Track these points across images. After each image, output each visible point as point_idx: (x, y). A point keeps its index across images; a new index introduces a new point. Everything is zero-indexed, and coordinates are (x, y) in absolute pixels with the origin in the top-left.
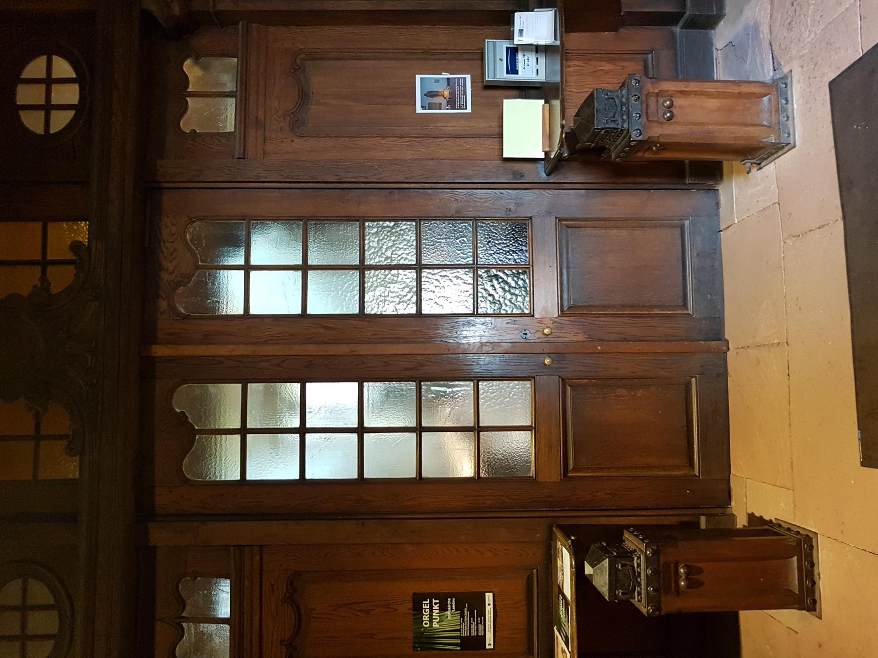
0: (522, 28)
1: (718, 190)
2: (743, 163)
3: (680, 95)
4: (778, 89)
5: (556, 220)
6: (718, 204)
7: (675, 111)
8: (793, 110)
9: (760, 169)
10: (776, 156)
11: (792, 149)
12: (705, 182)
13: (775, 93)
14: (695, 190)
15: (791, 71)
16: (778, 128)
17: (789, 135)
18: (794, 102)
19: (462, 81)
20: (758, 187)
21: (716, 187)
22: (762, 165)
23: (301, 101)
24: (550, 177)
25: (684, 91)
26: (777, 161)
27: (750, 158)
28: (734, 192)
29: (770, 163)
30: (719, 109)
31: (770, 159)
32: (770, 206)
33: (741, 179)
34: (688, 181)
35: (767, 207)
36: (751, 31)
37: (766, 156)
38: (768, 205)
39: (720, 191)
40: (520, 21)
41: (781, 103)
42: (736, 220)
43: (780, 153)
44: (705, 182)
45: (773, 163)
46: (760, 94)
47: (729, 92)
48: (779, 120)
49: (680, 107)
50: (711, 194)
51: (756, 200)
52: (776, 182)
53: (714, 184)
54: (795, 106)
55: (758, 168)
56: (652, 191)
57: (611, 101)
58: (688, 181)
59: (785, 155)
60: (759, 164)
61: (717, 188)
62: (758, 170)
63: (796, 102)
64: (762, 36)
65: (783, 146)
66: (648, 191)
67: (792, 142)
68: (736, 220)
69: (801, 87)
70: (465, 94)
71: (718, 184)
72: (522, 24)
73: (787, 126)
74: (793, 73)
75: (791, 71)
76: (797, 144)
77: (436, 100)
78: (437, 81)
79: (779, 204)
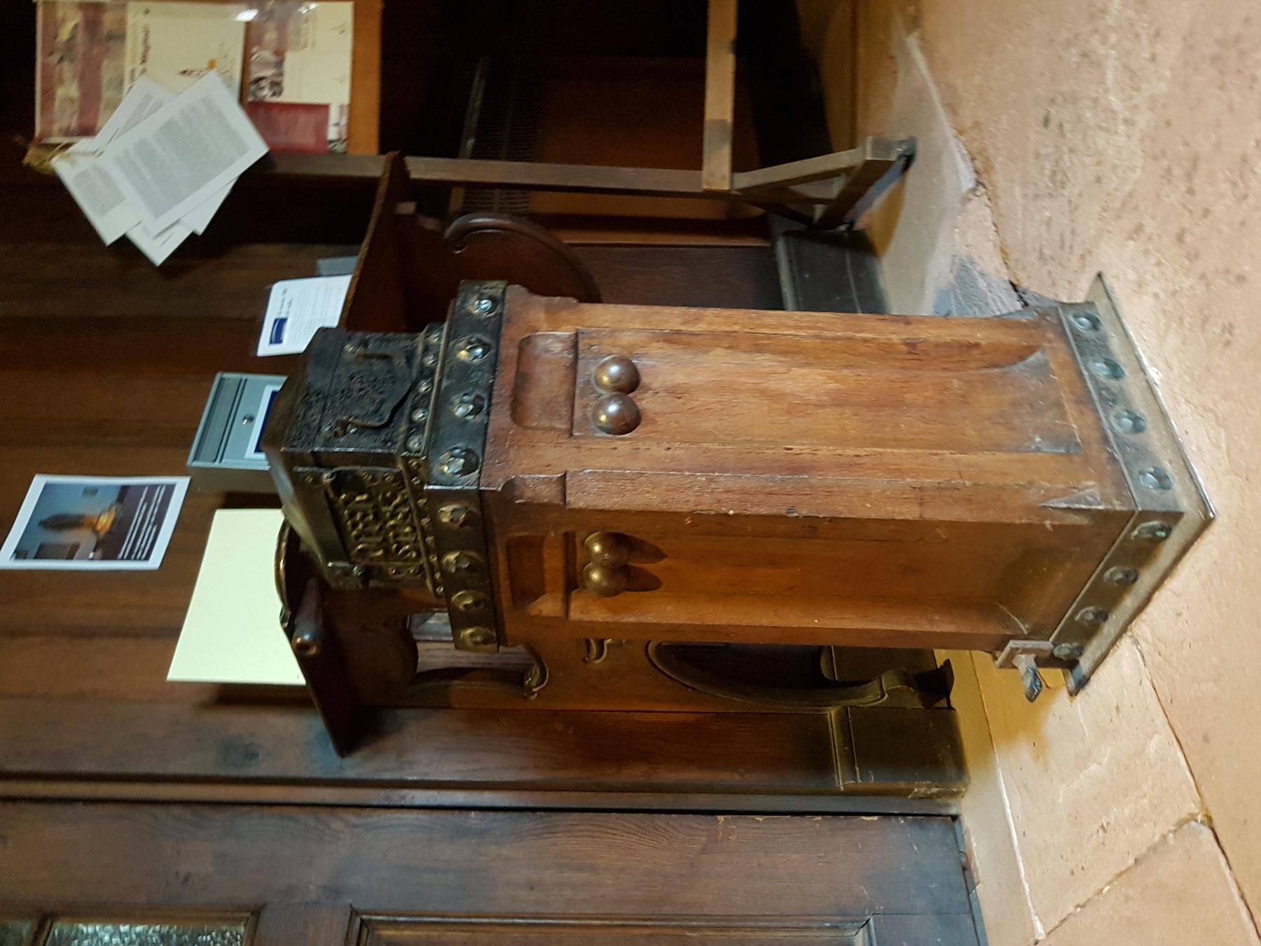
0: (283, 316)
1: (955, 818)
2: (1002, 656)
3: (668, 349)
4: (1064, 334)
5: (350, 921)
6: (965, 868)
7: (646, 402)
8: (1150, 387)
9: (1082, 683)
10: (1129, 603)
11: (1197, 535)
12: (902, 785)
13: (1060, 345)
14: (876, 818)
15: (1099, 276)
16: (1104, 456)
17: (1162, 480)
18: (1145, 362)
19: (158, 496)
20: (1093, 767)
21: (948, 806)
22: (1085, 663)
23: (542, 828)
24: (348, 762)
25: (679, 332)
26: (1141, 627)
27: (1024, 628)
28: (1009, 811)
29: (1113, 643)
30: (838, 401)
31: (1109, 628)
32: (1164, 837)
33: (1023, 752)
34: (841, 781)
35: (1154, 849)
36: (953, 302)
37: (1089, 613)
38: (1157, 839)
39: (968, 821)
40: (283, 300)
41: (1092, 376)
42: (1038, 925)
43: (1147, 578)
44: (902, 785)
45: (1125, 643)
46: (996, 348)
47: (865, 340)
48: (1102, 430)
49: (675, 392)
50: (936, 830)
51: (1097, 826)
52: (1161, 720)
53: (938, 795)
54: (1154, 374)
55: (1072, 684)
56: (721, 818)
57: (378, 365)
58: (841, 781)
59: (1172, 584)
60: (1070, 664)
61: (953, 811)
62: (1073, 694)
63: (1150, 359)
64: (982, 283)
65: (1153, 530)
66: (710, 818)
67: (1186, 504)
68: (1038, 925)
69: (1156, 296)
70: (159, 521)
71: (954, 795)
72: (285, 306)
73: (1142, 453)
74: (1109, 280)
75: (1099, 276)
76: (1214, 504)
77: (68, 537)
78: (91, 491)
79: (1209, 822)
